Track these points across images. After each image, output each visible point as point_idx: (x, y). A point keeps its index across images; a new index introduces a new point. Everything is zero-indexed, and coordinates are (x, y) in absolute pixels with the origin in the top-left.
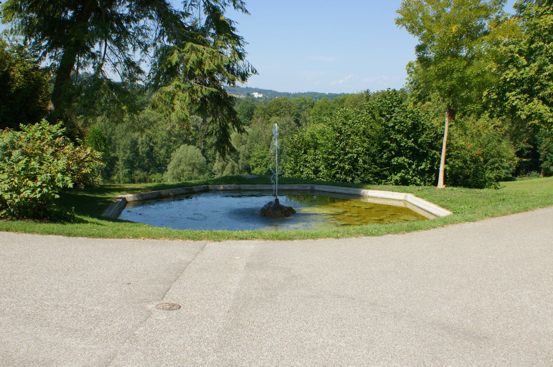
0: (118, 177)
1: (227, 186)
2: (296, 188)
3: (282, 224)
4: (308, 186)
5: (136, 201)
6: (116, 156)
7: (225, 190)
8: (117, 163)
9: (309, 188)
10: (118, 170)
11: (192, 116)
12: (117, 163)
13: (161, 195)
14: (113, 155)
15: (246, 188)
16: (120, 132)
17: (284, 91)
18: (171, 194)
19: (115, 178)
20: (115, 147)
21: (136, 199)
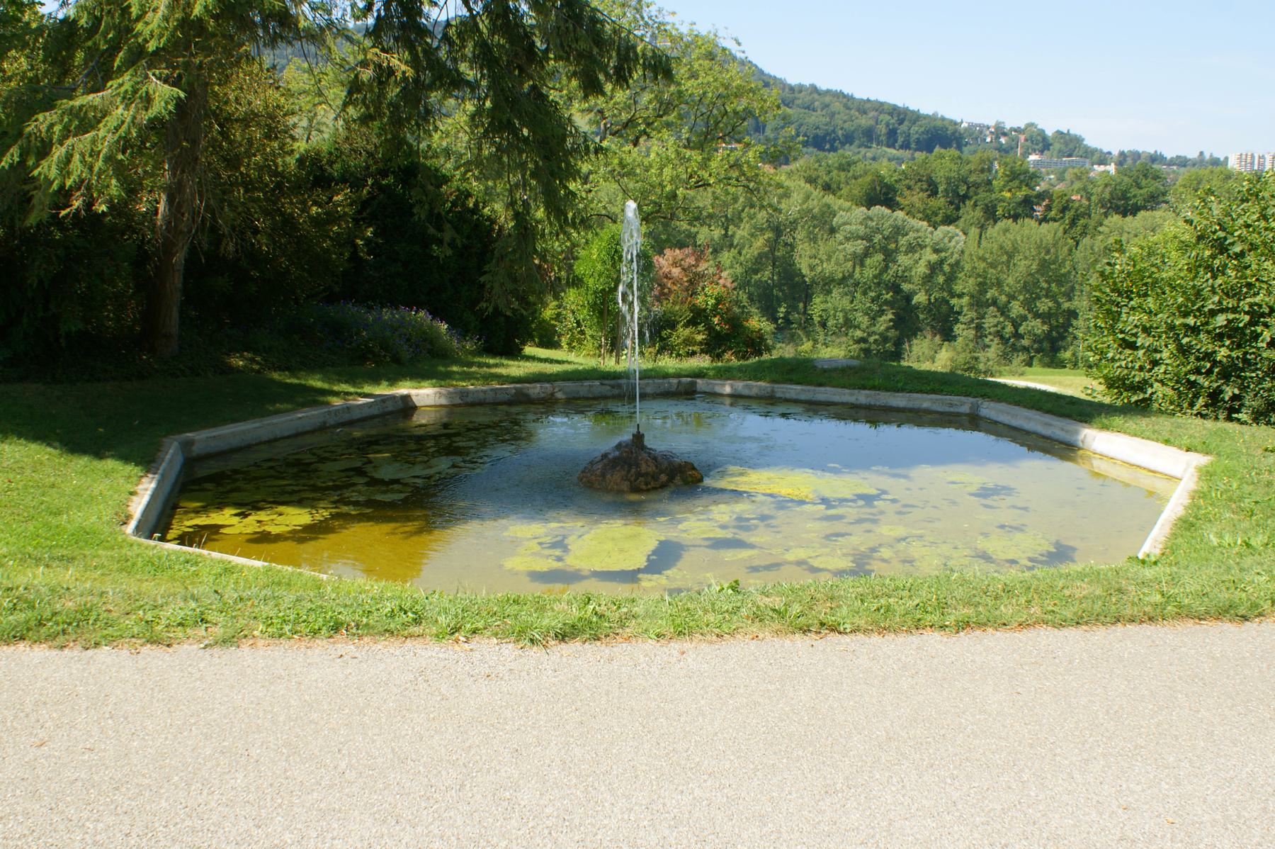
0: (1074, 354)
1: (740, 386)
2: (926, 405)
3: (675, 507)
4: (963, 404)
5: (441, 406)
6: (1072, 308)
7: (736, 397)
8: (1074, 322)
9: (965, 409)
10: (1075, 338)
11: (688, 153)
12: (1074, 322)
13: (526, 395)
14: (1066, 305)
15: (788, 396)
16: (1085, 257)
17: (835, 87)
18: (559, 395)
19: (1067, 355)
20: (1073, 289)
21: (444, 401)
